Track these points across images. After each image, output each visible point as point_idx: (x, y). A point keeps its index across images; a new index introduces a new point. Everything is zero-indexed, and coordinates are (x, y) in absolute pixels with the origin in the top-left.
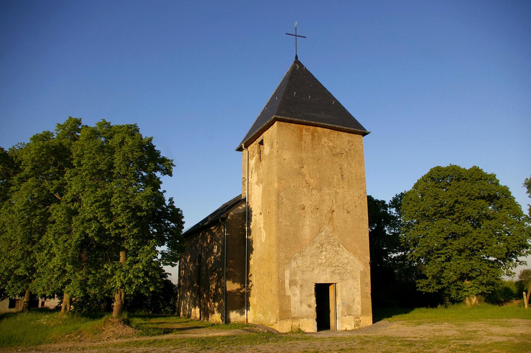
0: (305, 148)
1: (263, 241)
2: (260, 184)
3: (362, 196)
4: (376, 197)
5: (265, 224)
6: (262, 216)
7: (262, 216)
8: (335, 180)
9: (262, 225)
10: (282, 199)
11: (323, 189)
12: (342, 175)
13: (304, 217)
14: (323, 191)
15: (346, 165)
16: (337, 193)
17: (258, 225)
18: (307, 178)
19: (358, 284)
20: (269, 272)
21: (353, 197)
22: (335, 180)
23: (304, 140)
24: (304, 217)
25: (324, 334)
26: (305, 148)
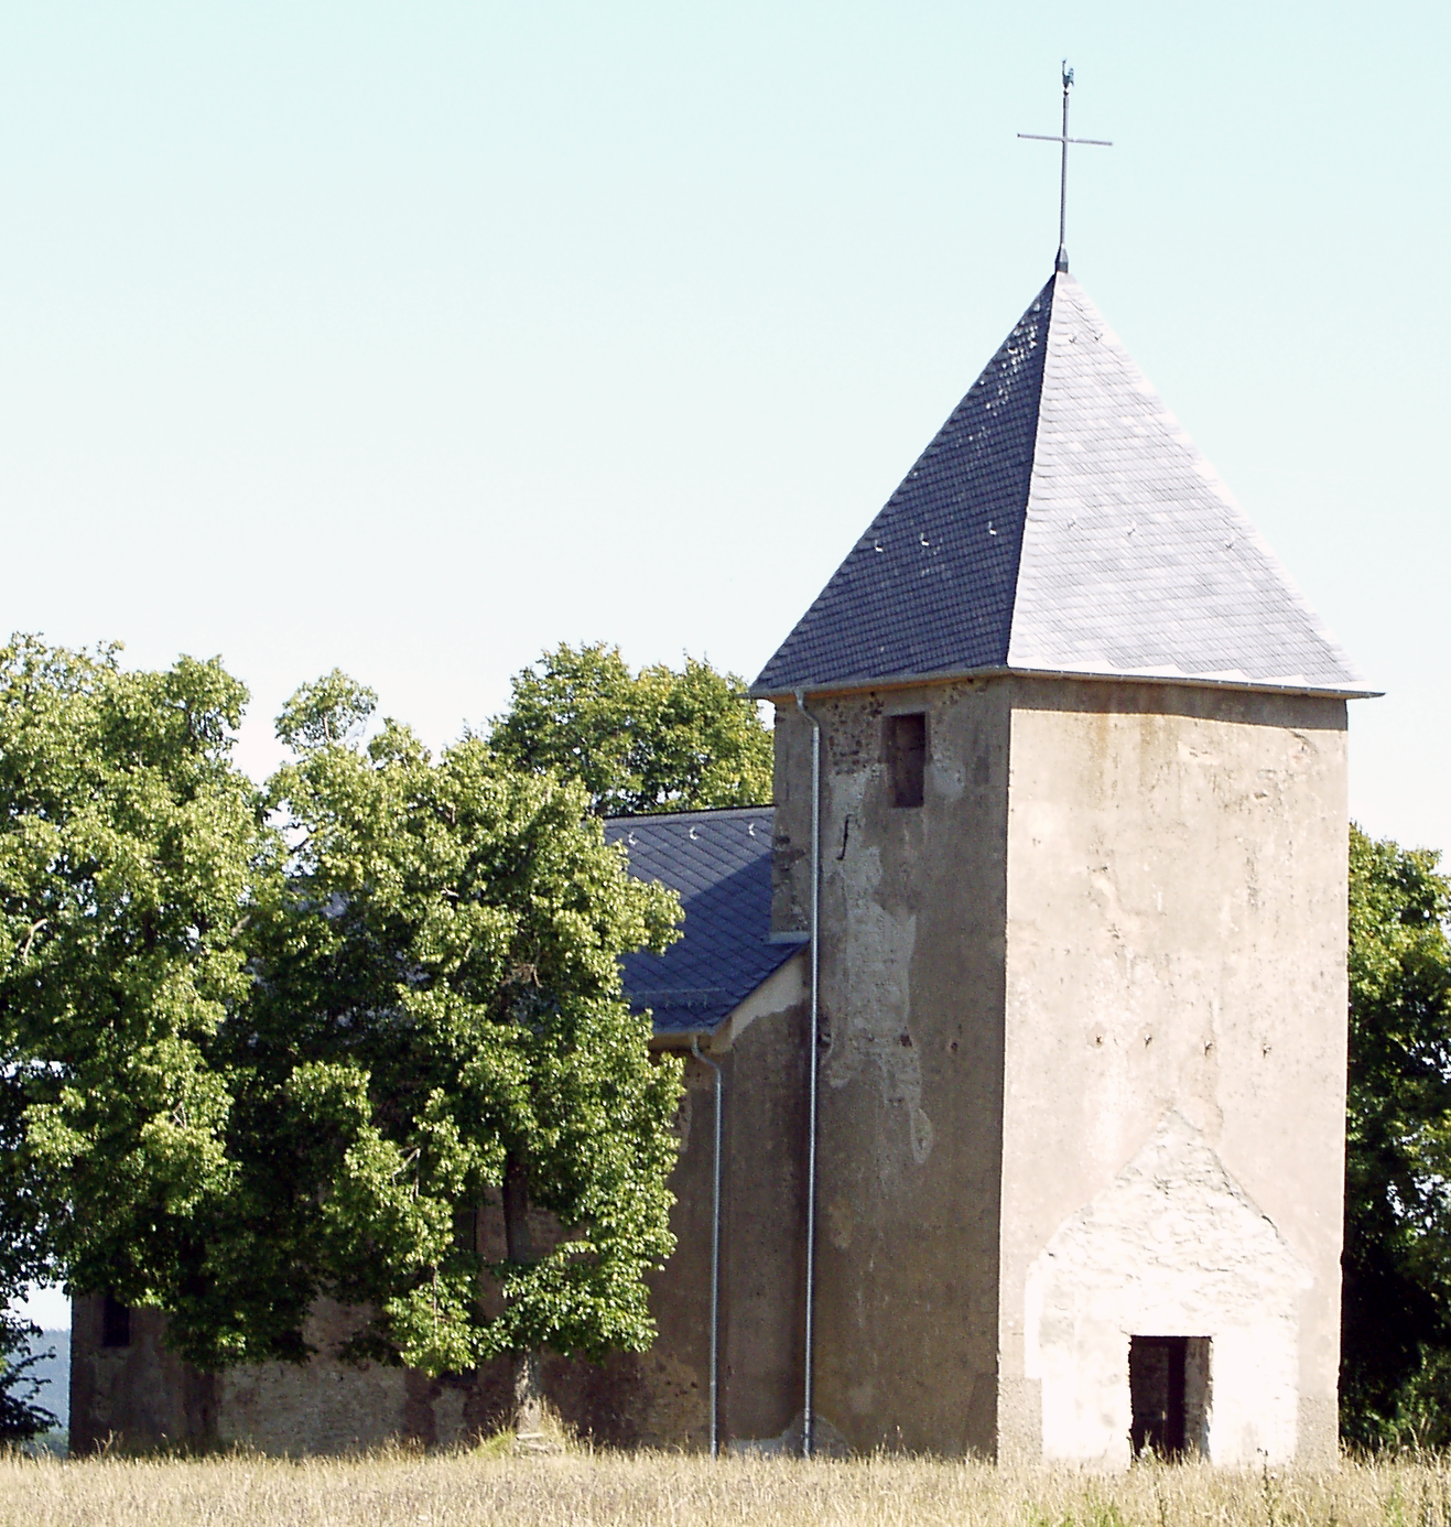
0: (1115, 784)
1: (920, 1157)
2: (902, 911)
3: (1328, 978)
4: (1375, 835)
5: (929, 1089)
6: (914, 1052)
7: (914, 1052)
8: (1225, 916)
9: (912, 1093)
10: (1023, 1003)
11: (1174, 956)
12: (1254, 892)
13: (1102, 1074)
14: (1174, 967)
15: (1270, 849)
16: (1227, 970)
17: (884, 1086)
18: (1113, 914)
19: (1003, 1414)
20: (949, 1287)
21: (1292, 982)
22: (1225, 916)
23: (1111, 752)
24: (1102, 1074)
25: (1186, 1477)
26: (1115, 784)
